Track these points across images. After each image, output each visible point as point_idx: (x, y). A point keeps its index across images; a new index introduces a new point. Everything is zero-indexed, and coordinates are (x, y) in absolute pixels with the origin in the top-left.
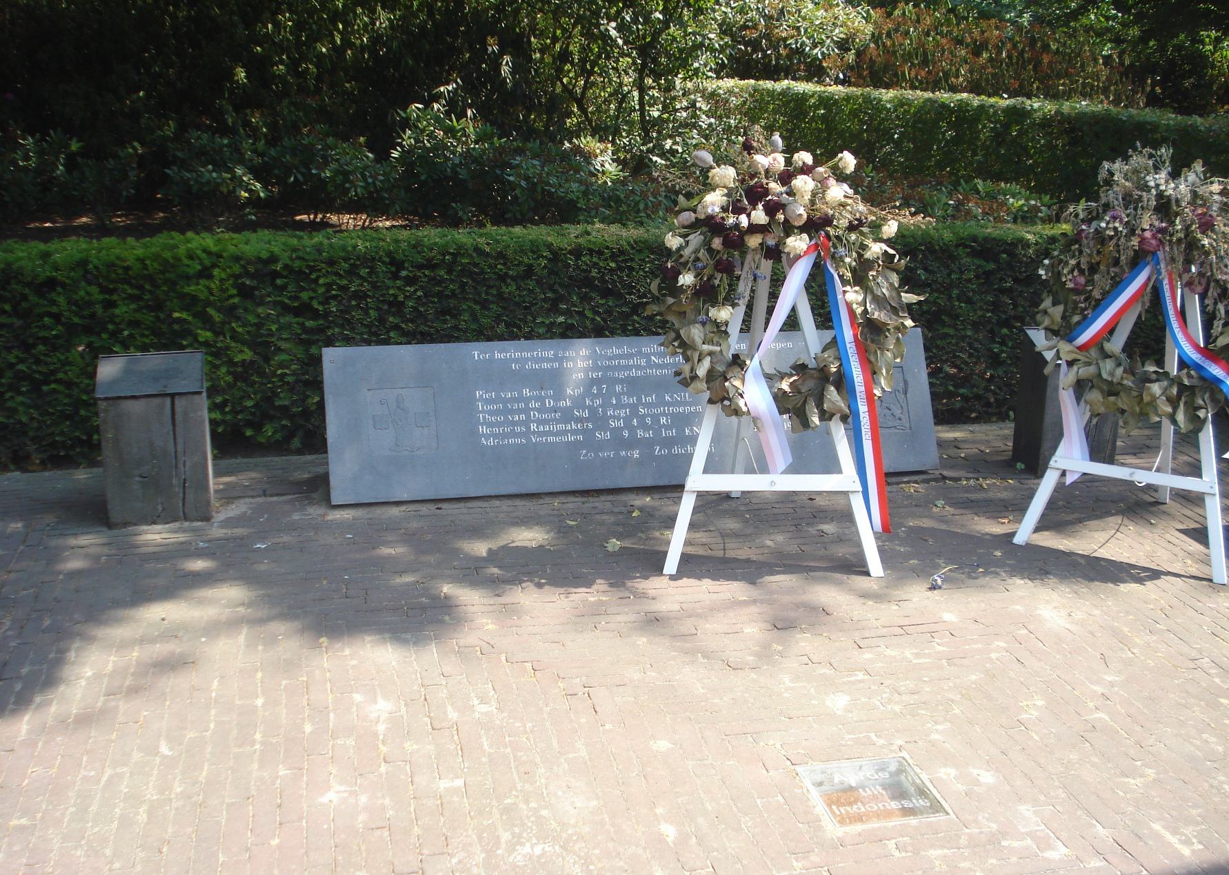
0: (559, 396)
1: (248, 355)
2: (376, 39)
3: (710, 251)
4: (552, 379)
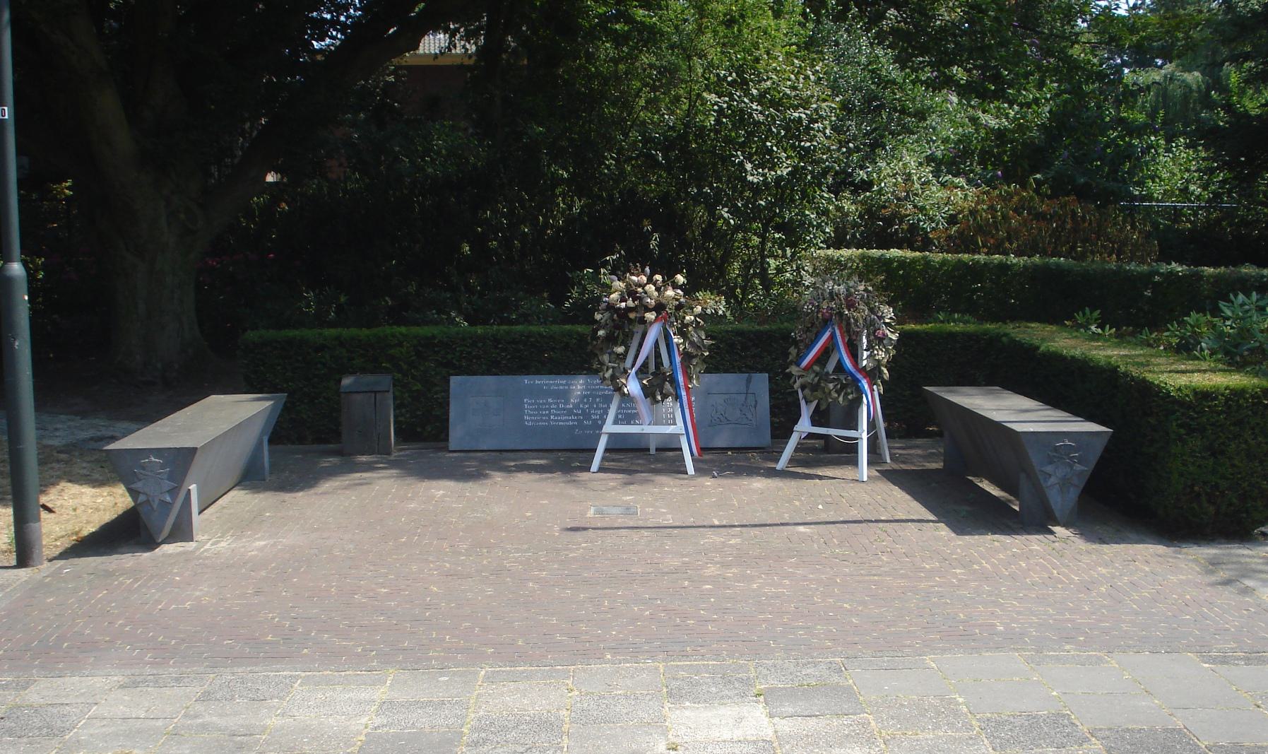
0: (567, 402)
1: (419, 386)
2: (570, 220)
3: (613, 320)
4: (564, 395)
